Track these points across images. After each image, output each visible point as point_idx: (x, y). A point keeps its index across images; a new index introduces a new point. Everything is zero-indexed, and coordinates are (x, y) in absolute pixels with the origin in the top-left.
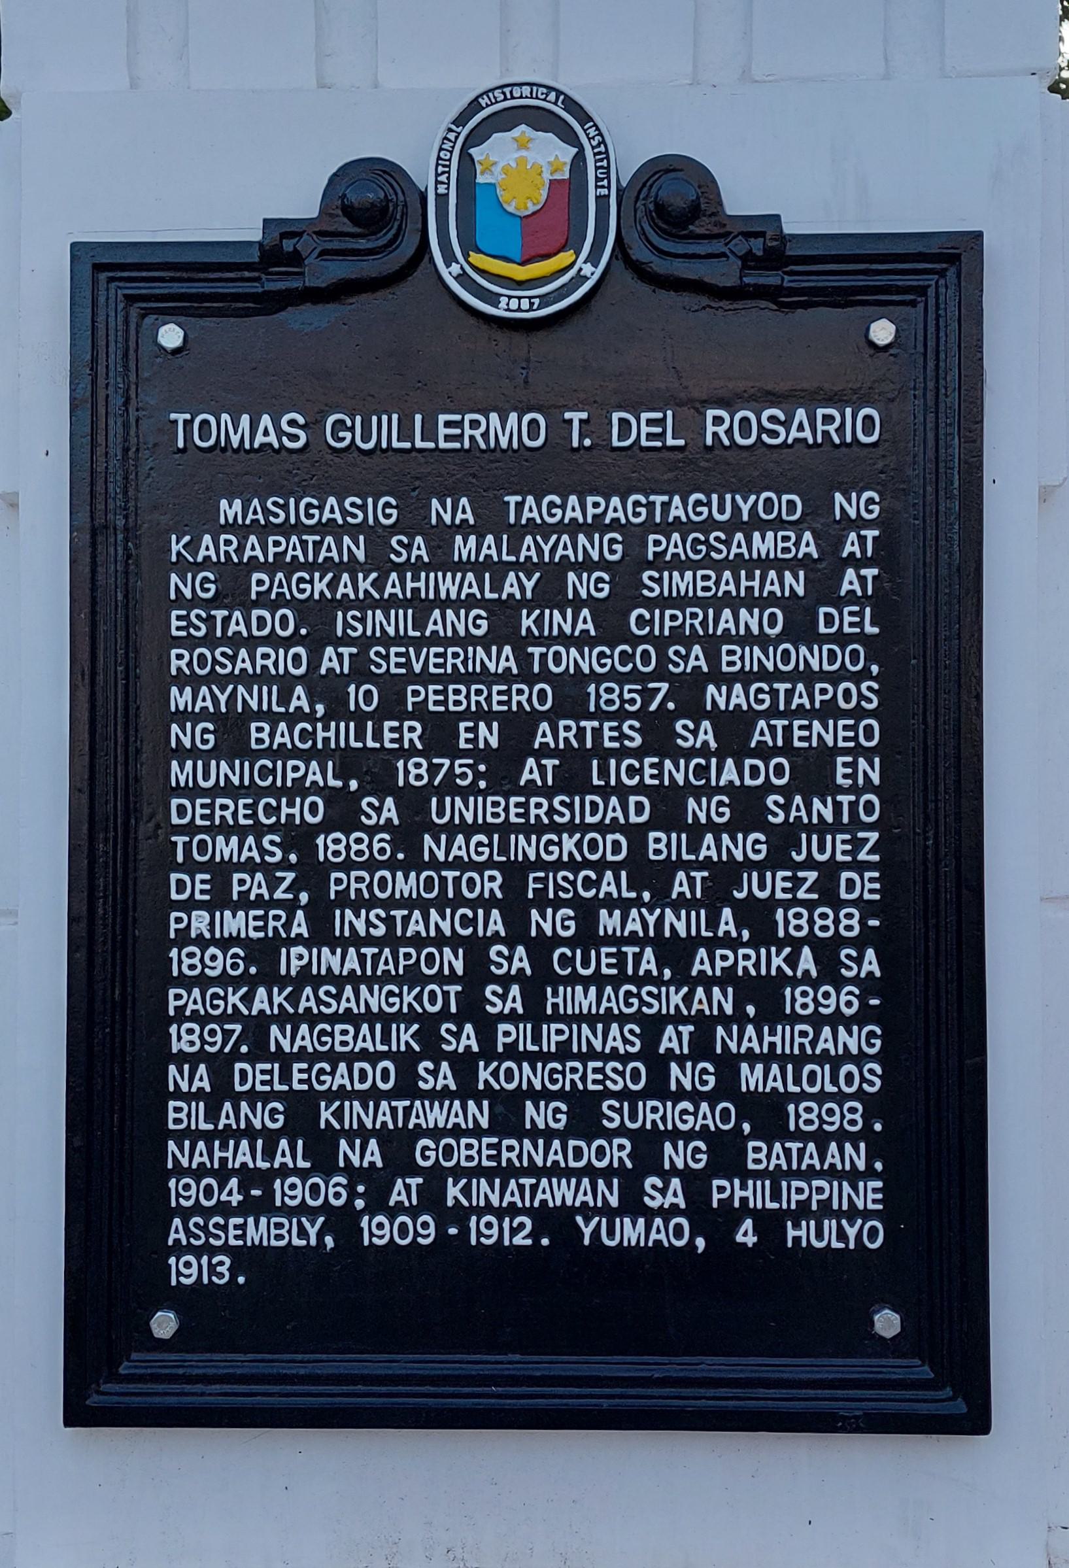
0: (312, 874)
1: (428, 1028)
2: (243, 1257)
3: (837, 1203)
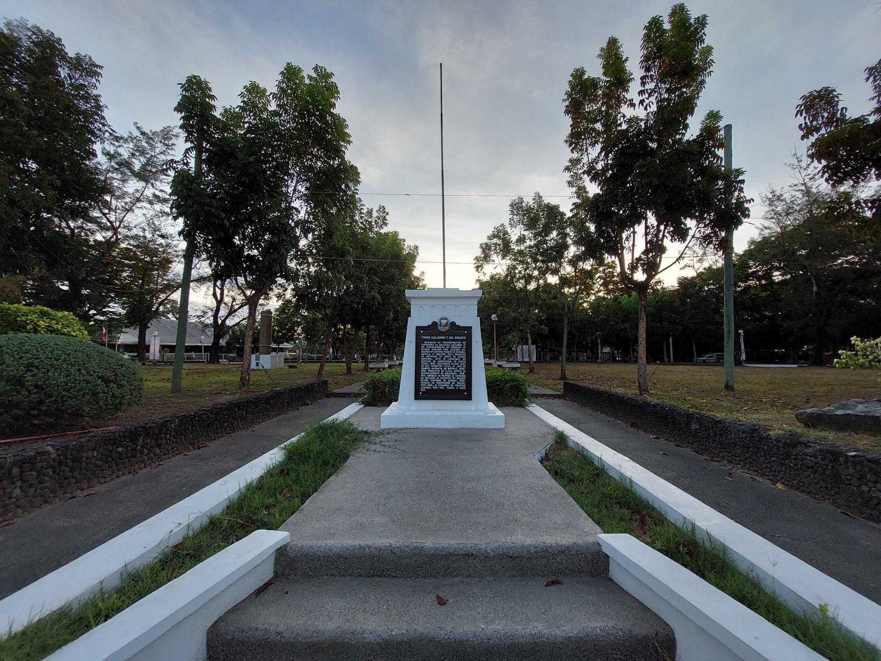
3: (463, 386)
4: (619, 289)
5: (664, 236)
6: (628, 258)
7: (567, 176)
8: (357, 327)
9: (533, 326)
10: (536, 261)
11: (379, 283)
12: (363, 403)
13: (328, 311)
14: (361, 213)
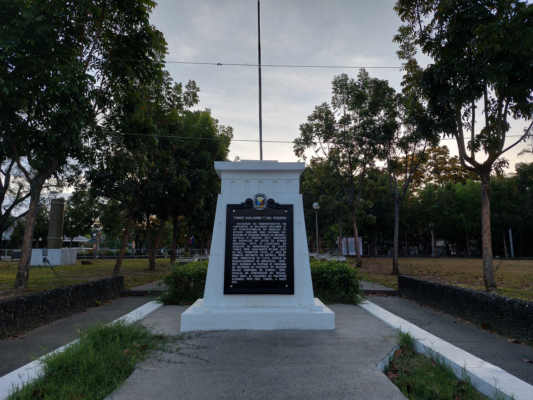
0: (243, 251)
1: (252, 263)
2: (238, 281)
3: (283, 276)
4: (451, 177)
5: (506, 111)
6: (467, 135)
7: (397, 46)
8: (163, 217)
9: (360, 215)
10: (361, 143)
11: (188, 167)
12: (162, 301)
13: (130, 198)
14: (168, 88)
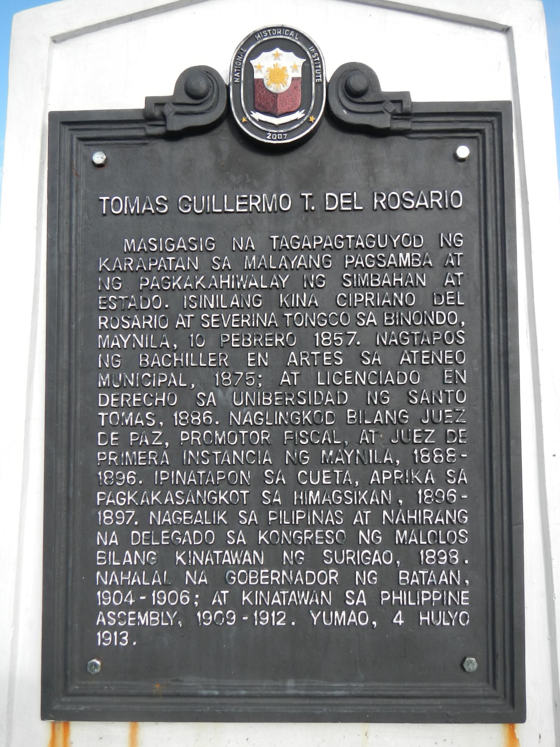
0: (171, 431)
2: (137, 631)
3: (443, 598)
